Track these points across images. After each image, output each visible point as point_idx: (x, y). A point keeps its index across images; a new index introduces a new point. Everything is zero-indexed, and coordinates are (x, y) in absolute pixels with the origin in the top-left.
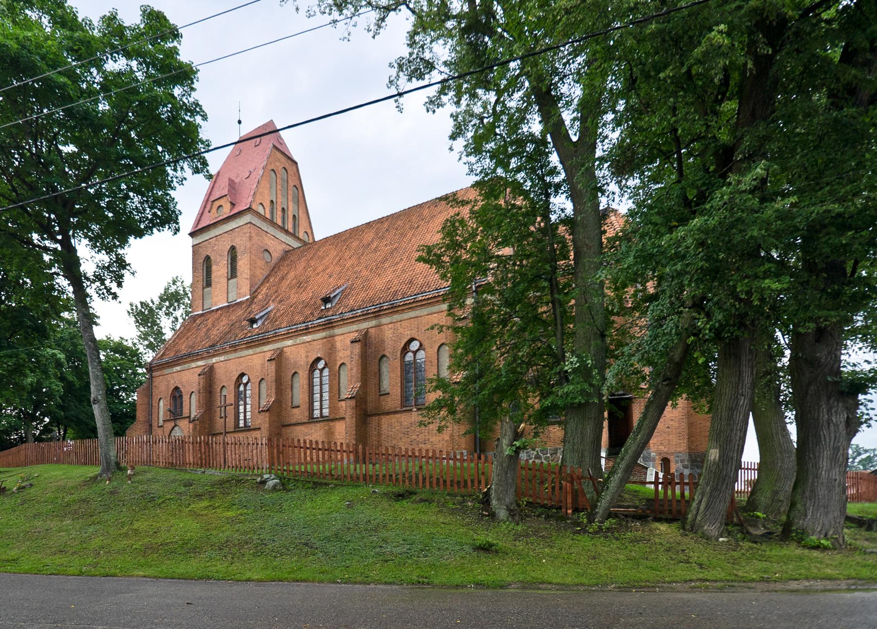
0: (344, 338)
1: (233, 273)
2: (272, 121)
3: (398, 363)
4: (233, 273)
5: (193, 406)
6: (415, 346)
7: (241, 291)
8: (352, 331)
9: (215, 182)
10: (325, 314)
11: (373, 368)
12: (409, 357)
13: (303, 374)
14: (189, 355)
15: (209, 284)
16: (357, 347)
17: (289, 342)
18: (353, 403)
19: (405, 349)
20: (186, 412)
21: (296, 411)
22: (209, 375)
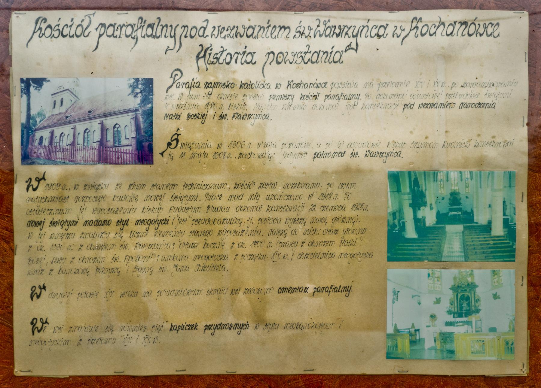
0: (95, 125)
1: (62, 105)
2: (152, 79)
3: (112, 131)
4: (62, 105)
5: (46, 142)
6: (117, 126)
7: (63, 110)
8: (98, 121)
9: (499, 19)
10: (90, 116)
11: (105, 132)
12: (116, 129)
13: (82, 134)
14: (47, 126)
15: (54, 107)
16: (100, 125)
17: (78, 124)
18: (99, 143)
19: (114, 127)
20: (43, 144)
21: (78, 146)
22: (52, 133)
